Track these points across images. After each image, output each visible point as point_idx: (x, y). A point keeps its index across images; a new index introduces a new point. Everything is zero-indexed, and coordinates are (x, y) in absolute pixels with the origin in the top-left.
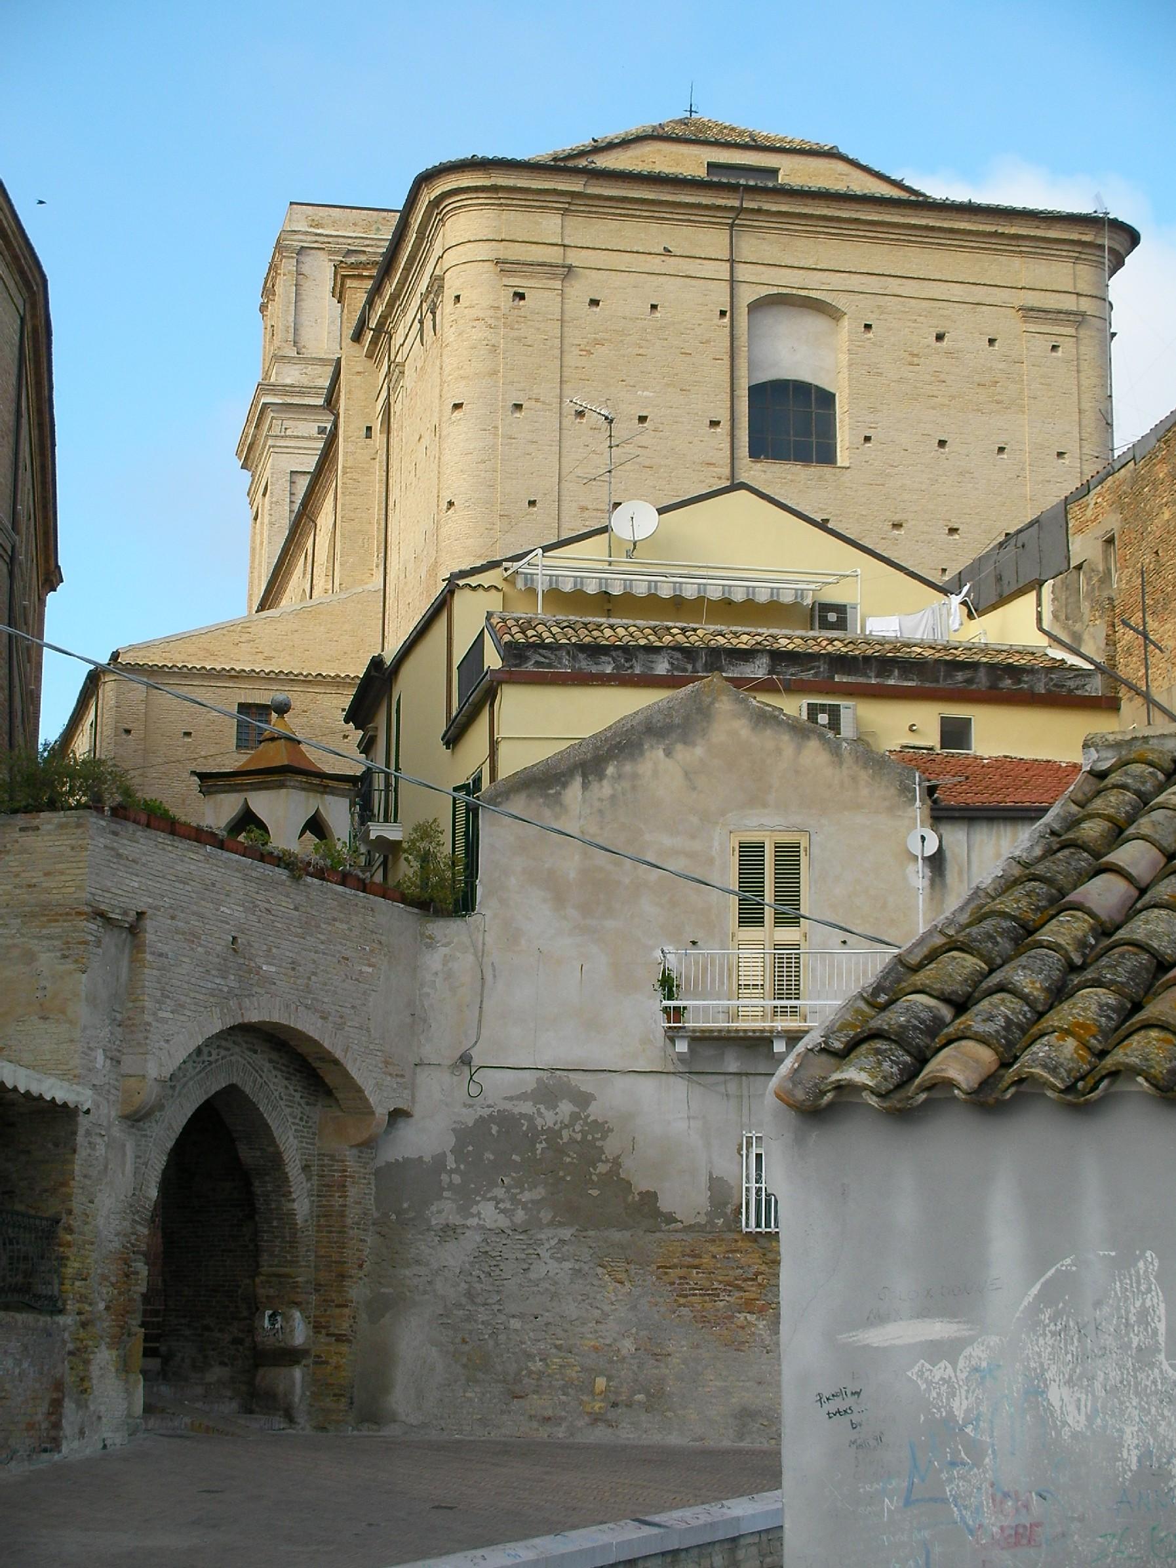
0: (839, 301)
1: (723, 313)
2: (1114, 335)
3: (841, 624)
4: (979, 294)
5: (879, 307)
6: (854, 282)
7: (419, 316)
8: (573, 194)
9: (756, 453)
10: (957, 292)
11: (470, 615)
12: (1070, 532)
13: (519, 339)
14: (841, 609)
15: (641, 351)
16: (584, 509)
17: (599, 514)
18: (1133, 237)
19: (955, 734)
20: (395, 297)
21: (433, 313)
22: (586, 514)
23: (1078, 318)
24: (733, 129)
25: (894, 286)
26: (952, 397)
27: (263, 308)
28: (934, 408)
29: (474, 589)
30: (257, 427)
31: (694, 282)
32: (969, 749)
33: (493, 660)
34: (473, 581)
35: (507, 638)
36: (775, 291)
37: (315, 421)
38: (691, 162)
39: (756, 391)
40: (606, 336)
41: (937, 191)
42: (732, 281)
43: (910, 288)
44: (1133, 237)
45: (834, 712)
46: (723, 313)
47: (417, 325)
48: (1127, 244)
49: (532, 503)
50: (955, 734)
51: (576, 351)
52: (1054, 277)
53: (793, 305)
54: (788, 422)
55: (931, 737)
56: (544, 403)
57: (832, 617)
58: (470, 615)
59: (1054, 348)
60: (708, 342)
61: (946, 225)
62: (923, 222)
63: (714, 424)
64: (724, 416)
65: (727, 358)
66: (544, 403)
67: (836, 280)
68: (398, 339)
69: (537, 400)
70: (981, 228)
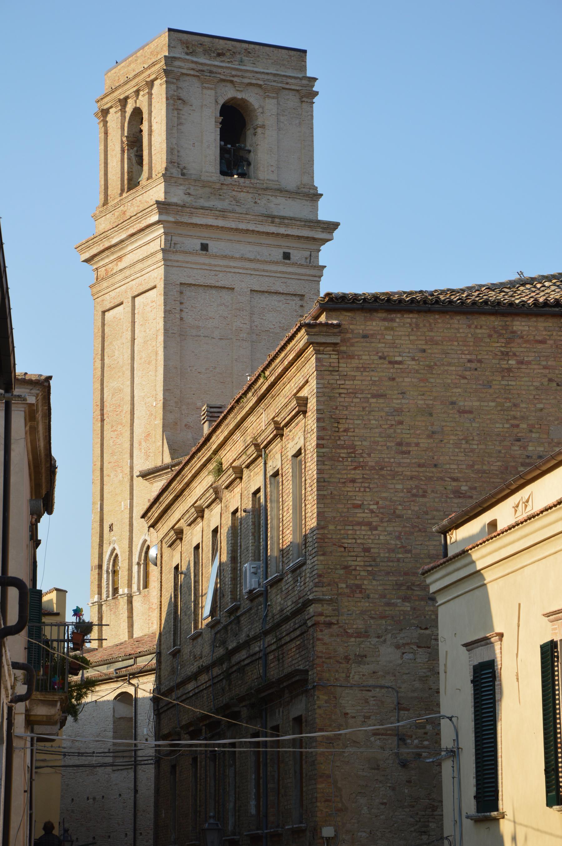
37: (199, 237)
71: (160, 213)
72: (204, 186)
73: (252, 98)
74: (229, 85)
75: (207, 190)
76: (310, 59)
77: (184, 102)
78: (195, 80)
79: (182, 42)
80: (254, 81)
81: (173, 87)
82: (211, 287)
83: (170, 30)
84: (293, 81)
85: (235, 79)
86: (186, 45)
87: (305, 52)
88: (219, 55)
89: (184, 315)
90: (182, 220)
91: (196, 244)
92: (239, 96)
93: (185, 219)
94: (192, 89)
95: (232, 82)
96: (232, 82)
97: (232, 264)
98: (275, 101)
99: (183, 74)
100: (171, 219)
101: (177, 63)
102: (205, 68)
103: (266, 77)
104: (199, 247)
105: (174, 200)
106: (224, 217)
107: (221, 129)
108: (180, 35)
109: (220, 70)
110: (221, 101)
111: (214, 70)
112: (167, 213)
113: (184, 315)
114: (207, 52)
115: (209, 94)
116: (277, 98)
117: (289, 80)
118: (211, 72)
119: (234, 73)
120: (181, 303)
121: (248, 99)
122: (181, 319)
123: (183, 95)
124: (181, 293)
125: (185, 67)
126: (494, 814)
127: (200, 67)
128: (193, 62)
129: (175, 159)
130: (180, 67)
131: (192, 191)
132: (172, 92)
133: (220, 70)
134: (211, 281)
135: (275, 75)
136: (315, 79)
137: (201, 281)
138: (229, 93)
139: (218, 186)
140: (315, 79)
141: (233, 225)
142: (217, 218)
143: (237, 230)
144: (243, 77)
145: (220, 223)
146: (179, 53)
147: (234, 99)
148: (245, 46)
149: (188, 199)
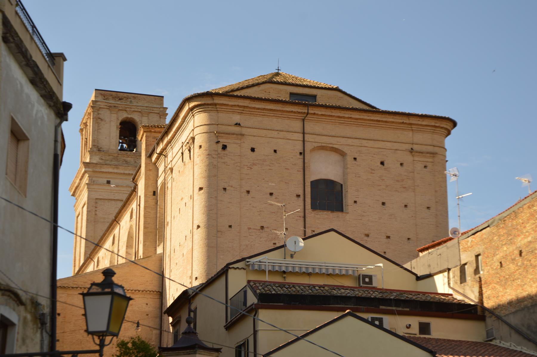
0: (345, 149)
1: (301, 153)
2: (447, 161)
3: (371, 282)
4: (396, 146)
5: (359, 151)
6: (350, 141)
7: (181, 151)
8: (244, 107)
9: (314, 207)
10: (389, 145)
11: (237, 280)
12: (461, 250)
13: (224, 163)
14: (370, 277)
15: (270, 168)
16: (249, 229)
17: (255, 231)
18: (455, 124)
19: (424, 328)
20: (169, 142)
21: (190, 151)
22: (250, 231)
23: (434, 154)
24: (296, 78)
25: (364, 142)
26: (387, 186)
27: (82, 130)
28: (380, 190)
29: (235, 269)
30: (81, 180)
31: (290, 141)
32: (429, 333)
33: (252, 299)
34: (235, 266)
35: (258, 291)
36: (320, 145)
37: (106, 178)
38: (283, 93)
39: (312, 183)
40: (257, 162)
41: (383, 108)
42: (304, 141)
43: (371, 144)
44: (455, 124)
45: (381, 320)
46: (301, 153)
47: (180, 153)
48: (452, 127)
49: (230, 226)
50: (424, 328)
51: (246, 168)
52: (423, 138)
53: (327, 150)
54: (327, 196)
55: (415, 330)
56: (234, 188)
57: (367, 280)
58: (237, 280)
59: (425, 167)
60: (295, 164)
61: (384, 120)
62: (376, 119)
63: (298, 196)
64: (301, 193)
65: (302, 170)
66: (234, 188)
67: (343, 141)
68: (170, 158)
69: (232, 186)
70: (398, 121)
71: (85, 168)
72: (109, 155)
73: (136, 117)
74: (125, 112)
75: (111, 157)
76: (165, 100)
77: (102, 120)
78: (107, 110)
79: (101, 94)
80: (136, 110)
81: (96, 113)
82: (112, 200)
83: (96, 90)
84: (156, 109)
85: (127, 109)
86: (104, 95)
87: (163, 97)
88: (120, 99)
89: (97, 213)
90: (96, 170)
91: (105, 181)
92: (129, 116)
93: (98, 169)
94: (105, 114)
95: (126, 110)
96: (126, 110)
97: (122, 189)
98: (147, 118)
99: (100, 108)
100: (90, 170)
101: (98, 103)
102: (112, 105)
103: (142, 108)
104: (106, 182)
105: (95, 162)
106: (117, 168)
107: (120, 131)
108: (112, 93)
109: (119, 106)
110: (120, 119)
111: (117, 105)
112: (89, 167)
113: (97, 213)
114: (114, 98)
115: (114, 116)
116: (148, 117)
117: (154, 109)
118: (115, 106)
119: (126, 106)
120: (96, 207)
121: (123, 117)
122: (96, 214)
123: (101, 116)
124: (96, 203)
125: (102, 105)
126: (479, 308)
127: (110, 105)
128: (106, 102)
129: (96, 144)
130: (99, 105)
131: (103, 158)
132: (95, 116)
133: (119, 106)
134: (112, 198)
135: (147, 107)
136: (167, 108)
137: (106, 197)
138: (124, 115)
139: (116, 155)
140: (167, 108)
141: (122, 172)
142: (114, 168)
143: (124, 174)
144: (131, 108)
145: (116, 171)
146: (100, 98)
147: (127, 118)
148: (109, 92)
149: (101, 161)
